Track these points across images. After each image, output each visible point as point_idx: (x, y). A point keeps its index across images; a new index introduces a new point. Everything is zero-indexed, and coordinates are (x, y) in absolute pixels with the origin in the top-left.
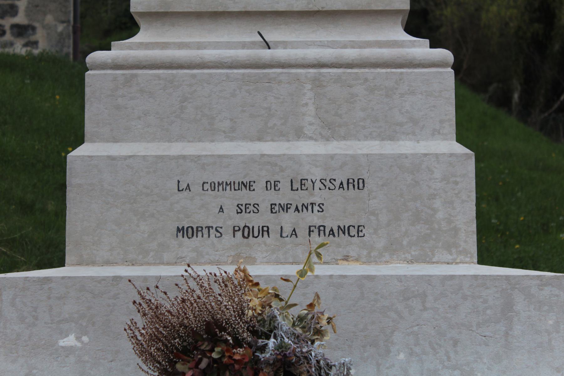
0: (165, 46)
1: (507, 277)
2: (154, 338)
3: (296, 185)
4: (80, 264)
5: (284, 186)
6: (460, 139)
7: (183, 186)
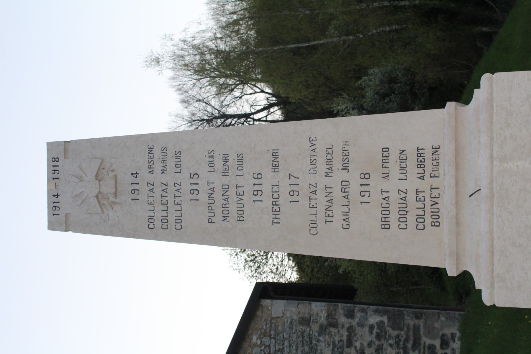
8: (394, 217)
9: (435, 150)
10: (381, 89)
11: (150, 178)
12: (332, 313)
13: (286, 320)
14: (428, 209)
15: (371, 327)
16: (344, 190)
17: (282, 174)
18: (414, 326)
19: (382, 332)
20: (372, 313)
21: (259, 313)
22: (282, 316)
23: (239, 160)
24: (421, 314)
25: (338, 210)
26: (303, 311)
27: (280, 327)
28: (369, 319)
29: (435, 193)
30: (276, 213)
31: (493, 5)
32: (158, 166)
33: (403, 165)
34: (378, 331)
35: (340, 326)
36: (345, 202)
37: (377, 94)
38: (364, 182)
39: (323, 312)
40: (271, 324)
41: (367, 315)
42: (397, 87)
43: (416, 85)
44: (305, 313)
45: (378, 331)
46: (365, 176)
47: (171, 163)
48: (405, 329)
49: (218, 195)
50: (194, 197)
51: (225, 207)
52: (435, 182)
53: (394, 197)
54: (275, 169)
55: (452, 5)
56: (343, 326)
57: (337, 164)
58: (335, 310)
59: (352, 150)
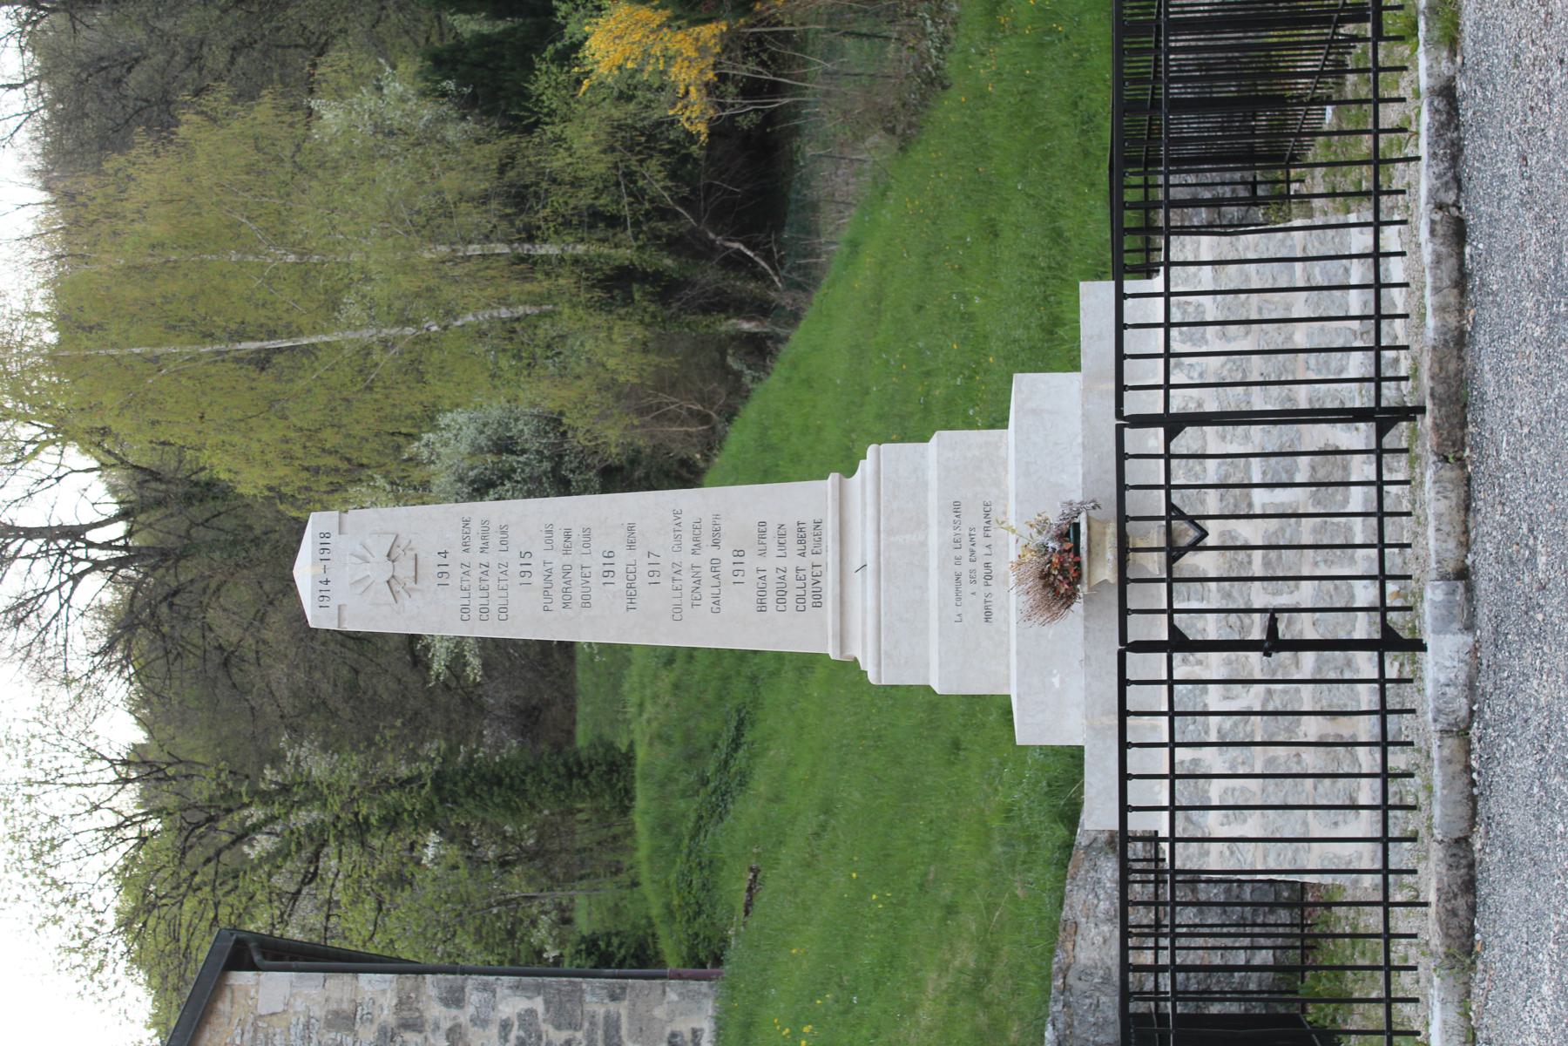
0: (864, 635)
1: (1016, 412)
2: (1049, 608)
3: (958, 545)
4: (1008, 685)
5: (958, 553)
6: (926, 439)
7: (958, 618)
8: (771, 599)
9: (818, 524)
10: (472, 469)
11: (465, 558)
12: (409, 997)
13: (294, 1021)
14: (809, 588)
15: (505, 1026)
16: (714, 569)
17: (640, 552)
18: (607, 1017)
19: (530, 1037)
20: (507, 992)
21: (224, 1006)
22: (285, 1011)
23: (585, 536)
24: (623, 989)
25: (706, 592)
26: (336, 995)
27: (277, 1037)
28: (500, 1007)
29: (817, 570)
30: (631, 597)
31: (767, 267)
32: (476, 543)
33: (782, 541)
34: (522, 1033)
35: (428, 1028)
36: (716, 582)
37: (461, 480)
38: (738, 559)
39: (388, 995)
40: (255, 1031)
41: (494, 996)
42: (518, 462)
43: (567, 458)
44: (342, 1000)
45: (522, 1033)
46: (739, 553)
47: (494, 539)
48: (586, 1025)
49: (558, 581)
50: (525, 580)
51: (565, 591)
52: (816, 559)
53: (772, 576)
54: (631, 545)
55: (668, 262)
56: (437, 1027)
57: (706, 540)
58: (417, 989)
59: (725, 526)
